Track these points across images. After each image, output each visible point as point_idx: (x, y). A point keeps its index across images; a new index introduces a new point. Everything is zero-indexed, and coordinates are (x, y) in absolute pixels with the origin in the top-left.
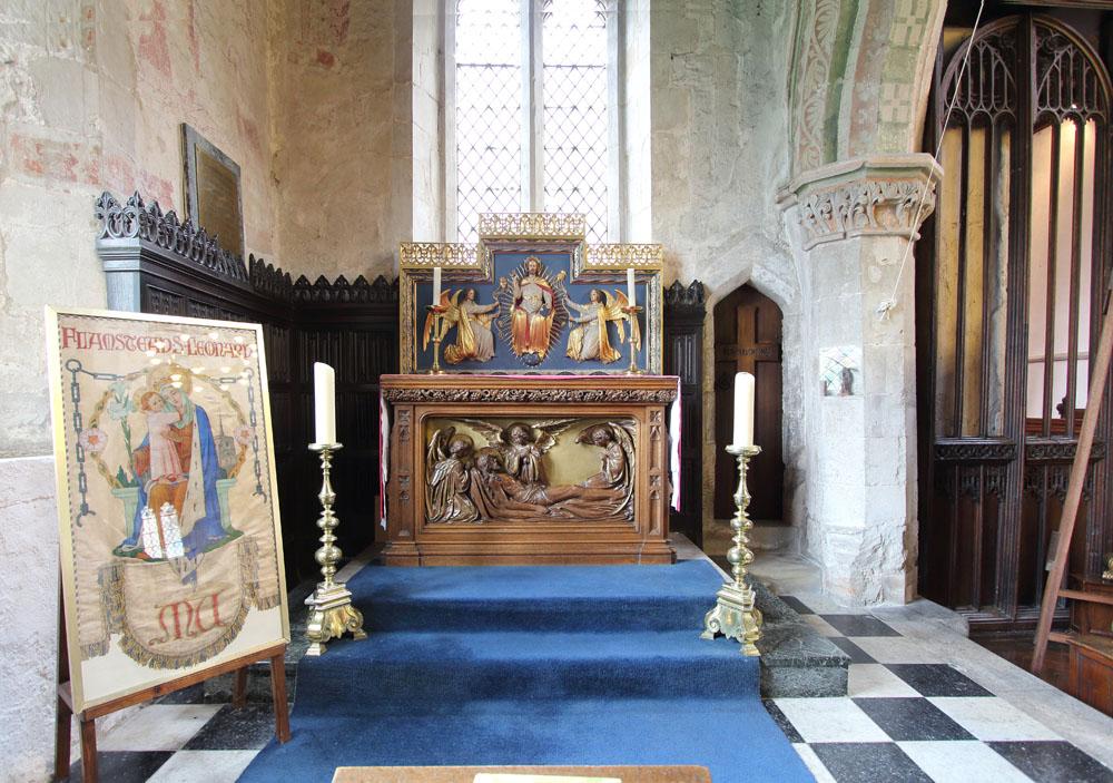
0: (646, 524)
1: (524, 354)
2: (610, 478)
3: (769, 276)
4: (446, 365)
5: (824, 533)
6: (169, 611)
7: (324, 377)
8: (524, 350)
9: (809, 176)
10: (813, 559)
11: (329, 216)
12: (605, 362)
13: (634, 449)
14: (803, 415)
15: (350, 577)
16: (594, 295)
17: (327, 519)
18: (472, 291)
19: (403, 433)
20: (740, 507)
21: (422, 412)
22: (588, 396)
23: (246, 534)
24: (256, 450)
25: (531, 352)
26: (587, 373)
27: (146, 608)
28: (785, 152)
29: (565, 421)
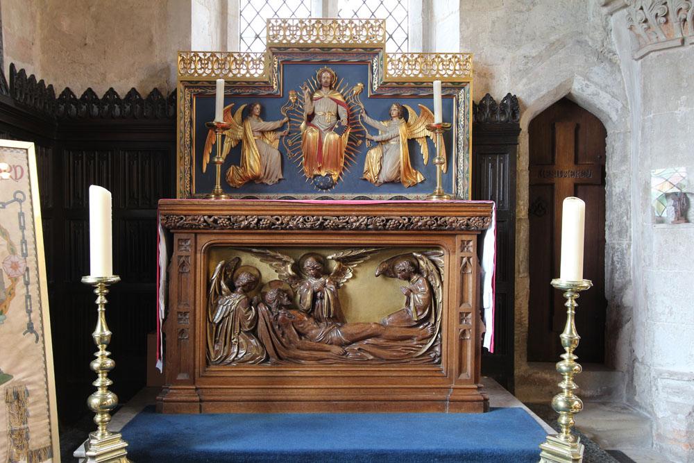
0: (455, 367)
1: (315, 176)
2: (414, 315)
3: (593, 88)
4: (228, 188)
7: (100, 200)
8: (316, 172)
10: (640, 407)
11: (97, 21)
12: (406, 185)
13: (442, 283)
14: (629, 245)
15: (122, 426)
16: (395, 110)
17: (102, 360)
18: (258, 106)
19: (183, 265)
20: (567, 349)
21: (204, 241)
23: (16, 378)
24: (27, 284)
25: (323, 174)
26: (386, 197)
29: (363, 251)
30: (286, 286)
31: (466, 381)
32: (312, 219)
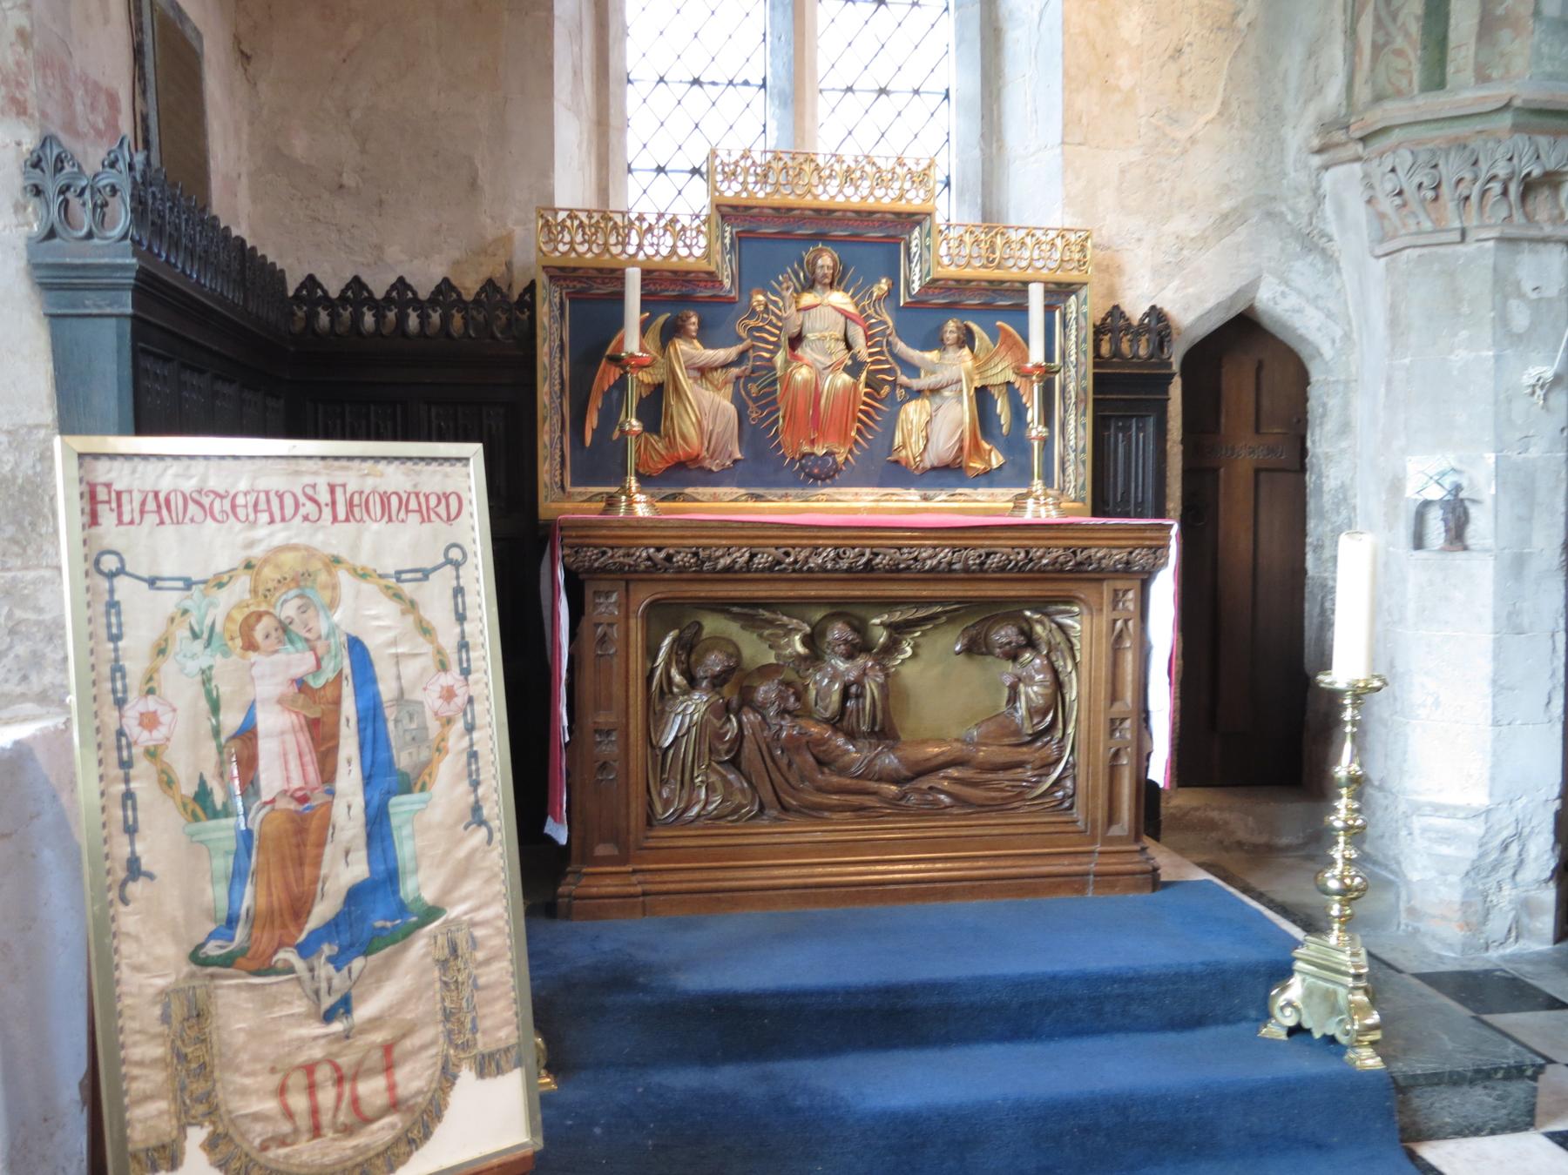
0: (1101, 815)
1: (804, 456)
2: (1027, 724)
3: (1293, 300)
5: (1407, 816)
6: (298, 1079)
8: (806, 449)
9: (1394, 111)
10: (1375, 863)
18: (694, 319)
19: (603, 640)
21: (643, 597)
22: (994, 561)
27: (253, 1074)
28: (1336, 53)
29: (939, 609)
30: (790, 675)
31: (1119, 840)
32: (851, 553)
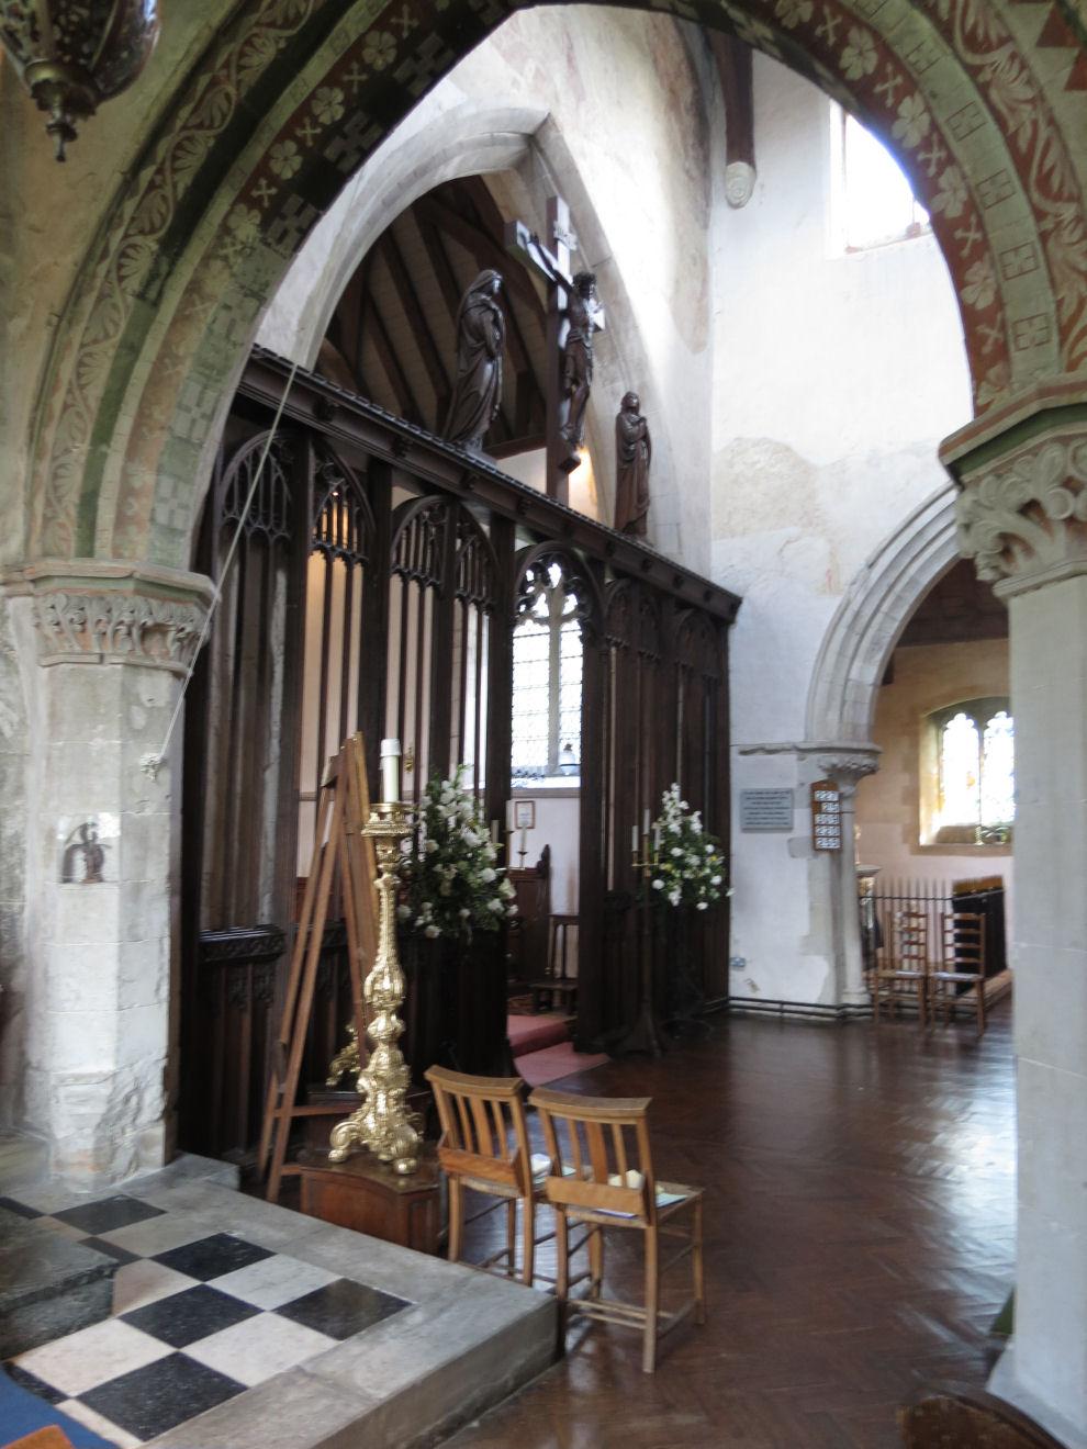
5: (55, 1087)
14: (22, 908)
